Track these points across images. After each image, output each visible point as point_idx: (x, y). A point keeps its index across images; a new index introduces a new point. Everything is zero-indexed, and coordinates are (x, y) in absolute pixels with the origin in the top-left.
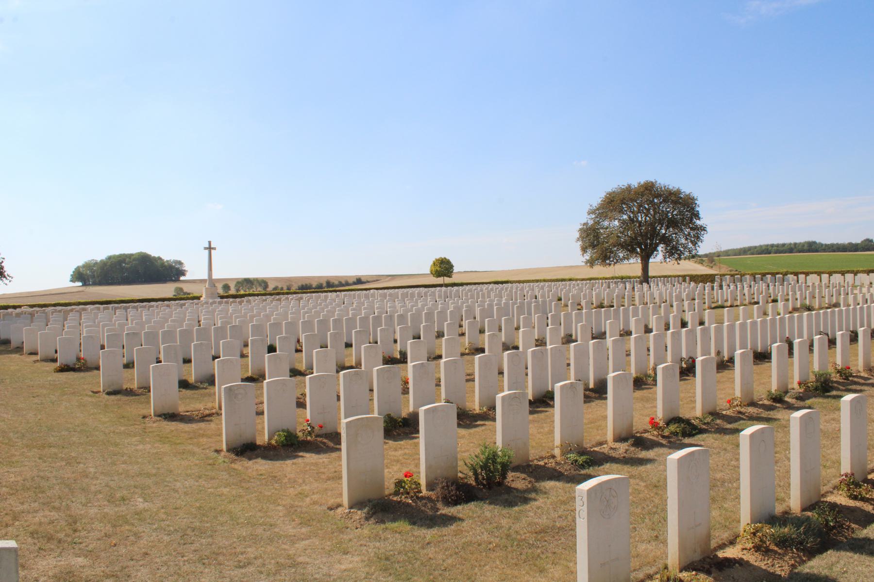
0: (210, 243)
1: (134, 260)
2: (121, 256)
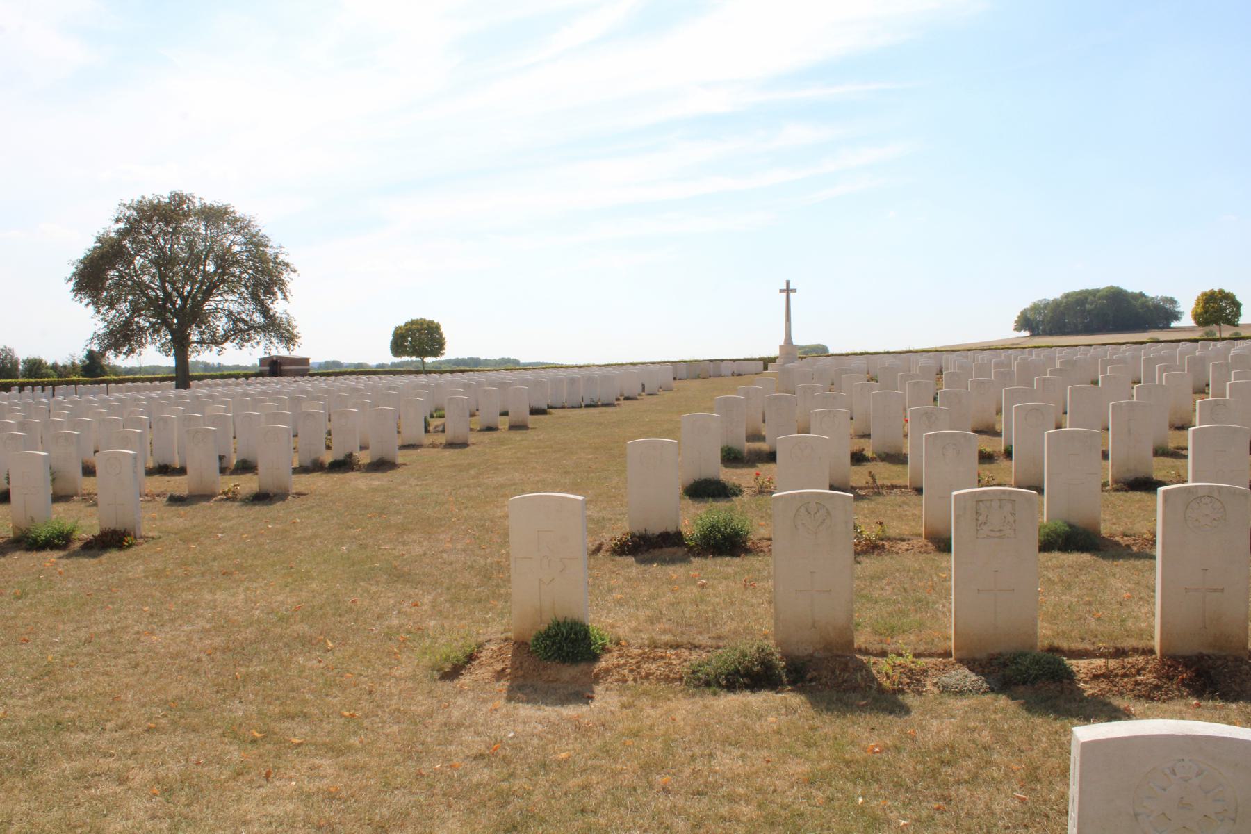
0: (788, 283)
1: (1100, 298)
2: (1082, 292)
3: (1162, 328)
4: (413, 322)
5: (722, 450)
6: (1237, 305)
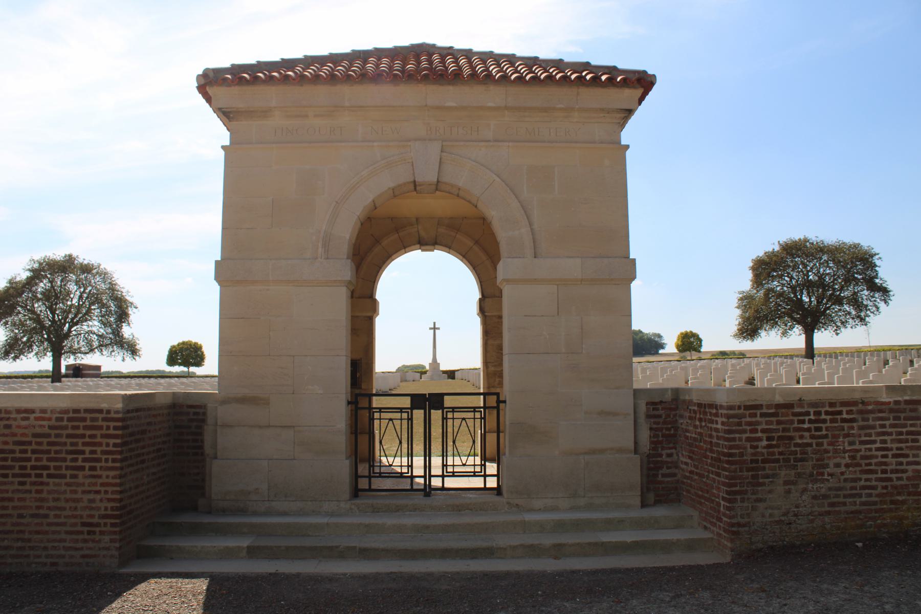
3: (654, 354)
4: (183, 343)
5: (654, 76)
6: (700, 340)
